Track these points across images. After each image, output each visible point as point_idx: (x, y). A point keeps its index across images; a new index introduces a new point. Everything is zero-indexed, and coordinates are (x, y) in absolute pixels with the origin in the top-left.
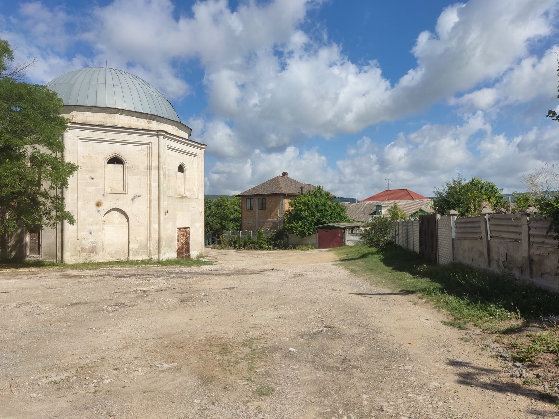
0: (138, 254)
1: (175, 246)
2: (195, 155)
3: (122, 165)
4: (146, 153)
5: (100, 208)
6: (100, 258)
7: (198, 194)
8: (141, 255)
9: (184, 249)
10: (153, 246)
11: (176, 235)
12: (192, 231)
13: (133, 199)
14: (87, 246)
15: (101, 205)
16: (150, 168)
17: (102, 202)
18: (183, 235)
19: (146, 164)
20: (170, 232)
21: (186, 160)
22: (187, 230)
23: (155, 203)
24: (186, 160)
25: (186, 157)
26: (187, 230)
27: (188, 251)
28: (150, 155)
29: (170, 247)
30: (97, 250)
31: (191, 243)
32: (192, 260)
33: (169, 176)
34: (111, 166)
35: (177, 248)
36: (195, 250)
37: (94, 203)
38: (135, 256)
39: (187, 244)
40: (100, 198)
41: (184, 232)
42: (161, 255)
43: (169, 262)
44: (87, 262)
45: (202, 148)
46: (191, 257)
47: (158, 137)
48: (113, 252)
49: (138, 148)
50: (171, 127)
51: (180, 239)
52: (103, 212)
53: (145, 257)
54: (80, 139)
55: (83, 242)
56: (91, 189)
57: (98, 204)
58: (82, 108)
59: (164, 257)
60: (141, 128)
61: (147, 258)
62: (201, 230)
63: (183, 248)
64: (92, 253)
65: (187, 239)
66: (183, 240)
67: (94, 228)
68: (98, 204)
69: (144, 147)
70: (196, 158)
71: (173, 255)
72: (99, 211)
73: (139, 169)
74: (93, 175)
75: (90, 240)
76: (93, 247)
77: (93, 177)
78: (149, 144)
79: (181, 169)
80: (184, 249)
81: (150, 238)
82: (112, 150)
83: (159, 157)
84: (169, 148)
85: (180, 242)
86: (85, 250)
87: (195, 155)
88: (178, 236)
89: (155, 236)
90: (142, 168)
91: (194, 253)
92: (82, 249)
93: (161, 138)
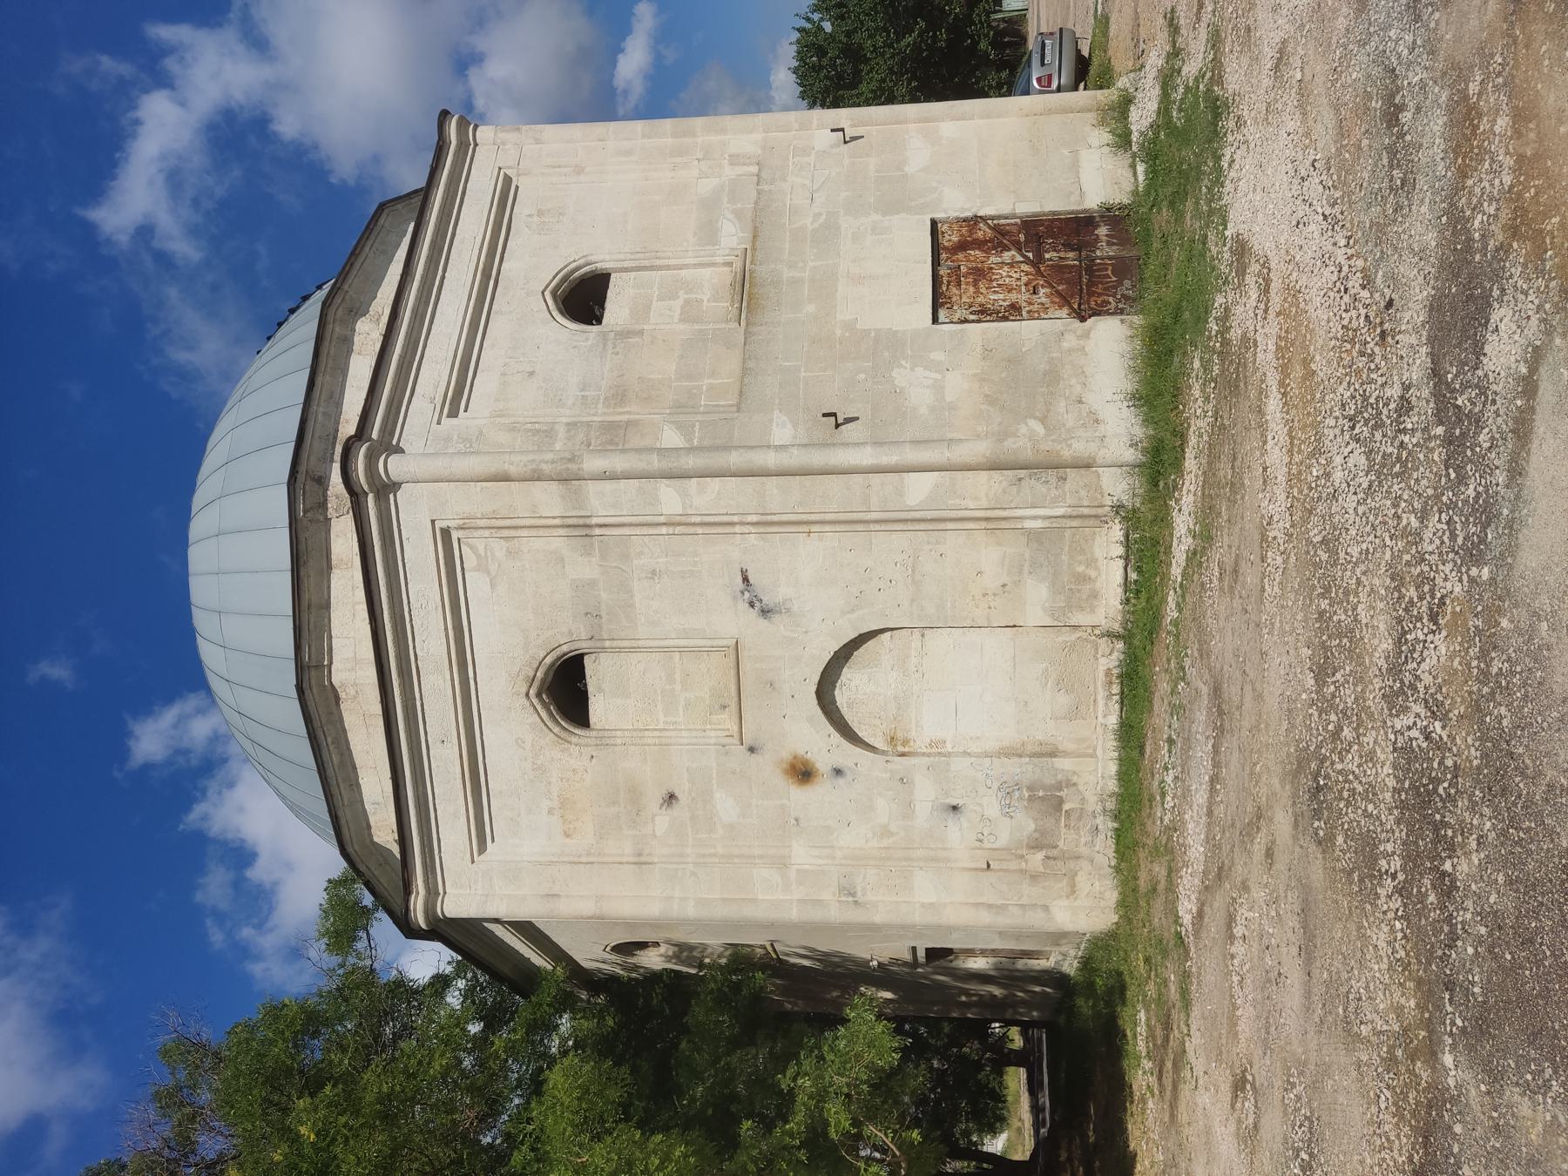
0: (1083, 579)
1: (1045, 332)
2: (506, 194)
3: (587, 660)
4: (499, 548)
5: (822, 763)
6: (1096, 772)
7: (735, 160)
8: (1092, 562)
9: (1073, 259)
10: (1040, 505)
12: (956, 204)
13: (765, 612)
14: (1026, 823)
15: (806, 763)
16: (582, 528)
17: (786, 755)
18: (980, 274)
19: (557, 542)
20: (950, 372)
22: (950, 238)
23: (778, 496)
24: (533, 266)
25: (513, 266)
26: (950, 238)
27: (1074, 229)
28: (505, 528)
29: (1052, 377)
30: (1050, 780)
31: (1028, 206)
32: (1150, 196)
33: (619, 396)
34: (597, 708)
35: (1060, 323)
36: (1075, 166)
37: (799, 796)
38: (1094, 595)
40: (768, 768)
41: (964, 259)
42: (1104, 455)
43: (1158, 391)
45: (463, 145)
46: (1121, 197)
47: (395, 486)
48: (1063, 700)
49: (476, 586)
51: (1000, 299)
52: (847, 754)
53: (1109, 544)
54: (482, 847)
55: (1003, 839)
56: (725, 806)
57: (803, 773)
58: (346, 815)
59: (1117, 430)
61: (1117, 531)
62: (948, 129)
63: (1059, 269)
64: (1061, 801)
67: (926, 793)
68: (803, 773)
70: (523, 183)
71: (1107, 347)
72: (838, 772)
73: (592, 583)
74: (654, 796)
75: (993, 808)
76: (1031, 799)
77: (664, 792)
78: (446, 533)
80: (1073, 259)
81: (993, 522)
83: (505, 478)
84: (455, 402)
85: (1022, 297)
86: (1043, 833)
87: (506, 194)
88: (985, 313)
89: (982, 489)
90: (584, 568)
91: (1098, 178)
92: (1036, 846)
93: (395, 467)
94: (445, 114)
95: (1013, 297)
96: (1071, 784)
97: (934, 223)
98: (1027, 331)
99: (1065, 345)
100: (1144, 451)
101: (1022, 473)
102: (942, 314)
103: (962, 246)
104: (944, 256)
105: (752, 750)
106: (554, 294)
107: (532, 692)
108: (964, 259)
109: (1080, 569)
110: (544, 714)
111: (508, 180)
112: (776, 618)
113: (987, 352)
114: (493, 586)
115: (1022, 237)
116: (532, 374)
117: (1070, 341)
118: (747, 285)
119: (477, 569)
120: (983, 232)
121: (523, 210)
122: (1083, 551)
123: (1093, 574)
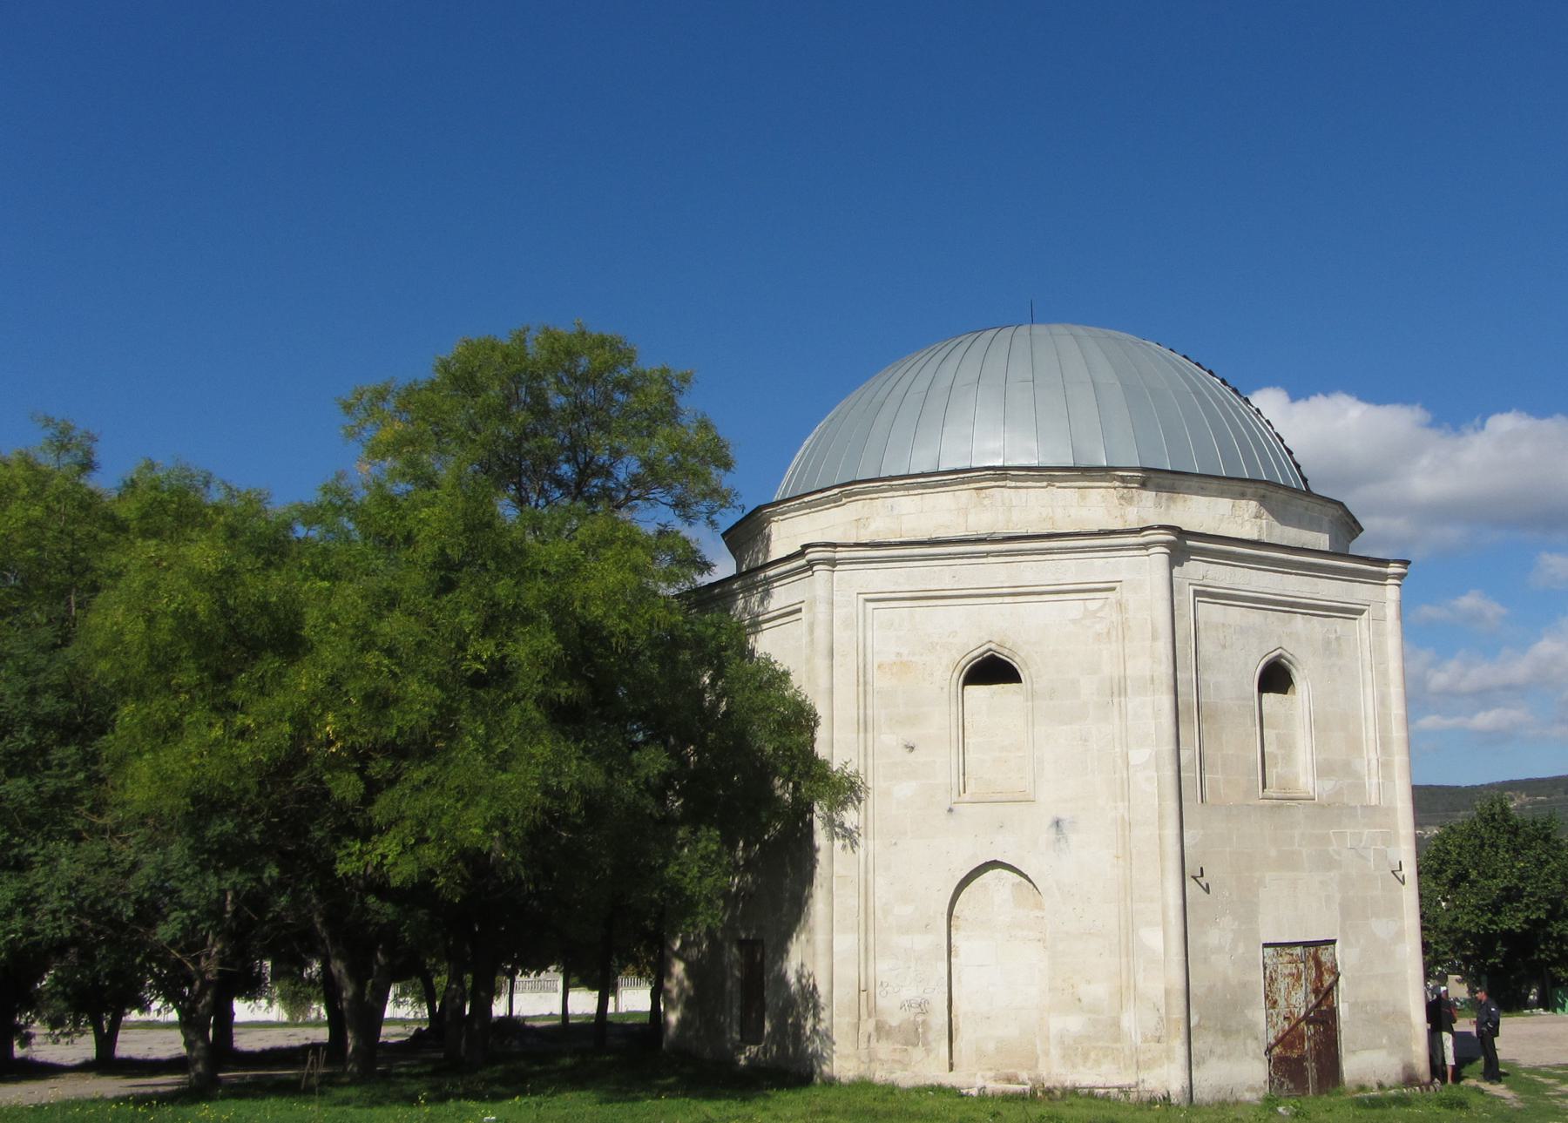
0: (1086, 1057)
1: (1261, 1024)
2: (1351, 612)
8: (1098, 1062)
11: (1258, 977)
12: (1345, 957)
21: (1295, 637)
22: (1324, 956)
24: (1295, 637)
25: (1299, 623)
34: (975, 691)
39: (1324, 1017)
44: (451, 1103)
45: (1146, 546)
49: (1073, 607)
50: (1224, 504)
60: (1095, 529)
65: (1324, 994)
66: (1299, 1000)
69: (1095, 603)
76: (915, 1023)
78: (1113, 589)
79: (1276, 677)
82: (973, 628)
88: (1271, 981)
92: (879, 1027)
94: (1406, 563)
95: (1282, 1002)
96: (928, 1052)
97: (1333, 942)
98: (1259, 1015)
99: (1249, 1041)
100: (273, 760)
101: (1163, 1011)
102: (1270, 950)
103: (1318, 964)
104: (1312, 950)
105: (950, 810)
106: (1280, 656)
107: (993, 646)
108: (1315, 957)
109: (1093, 1055)
110: (976, 653)
111: (1361, 612)
112: (1053, 830)
113: (1244, 985)
114: (1074, 621)
115: (1324, 1008)
116: (1224, 647)
117: (1252, 1045)
118: (1289, 803)
119: (1086, 609)
120: (1328, 979)
121: (1338, 625)
122: (1105, 1056)
123: (1089, 1064)
